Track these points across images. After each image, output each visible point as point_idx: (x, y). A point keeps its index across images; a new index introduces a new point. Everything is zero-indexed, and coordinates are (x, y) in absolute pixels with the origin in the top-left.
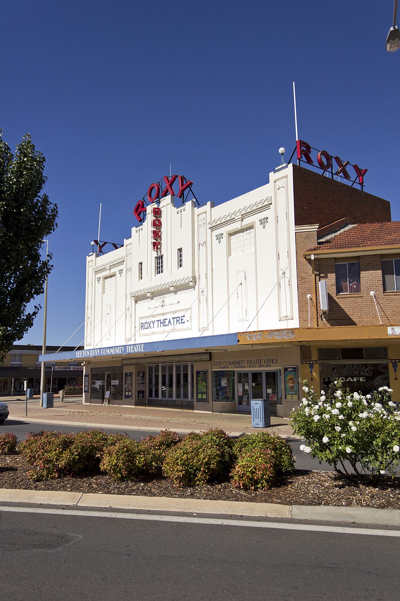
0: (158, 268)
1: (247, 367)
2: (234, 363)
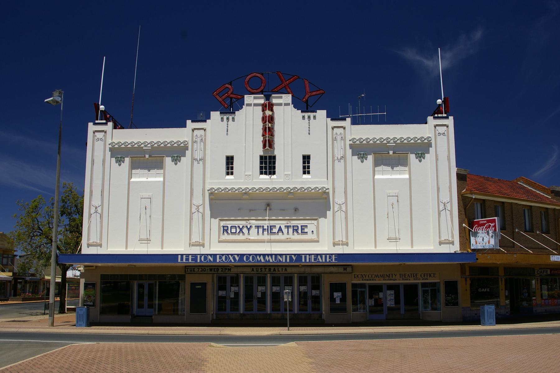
0: (304, 167)
1: (399, 280)
2: (383, 276)
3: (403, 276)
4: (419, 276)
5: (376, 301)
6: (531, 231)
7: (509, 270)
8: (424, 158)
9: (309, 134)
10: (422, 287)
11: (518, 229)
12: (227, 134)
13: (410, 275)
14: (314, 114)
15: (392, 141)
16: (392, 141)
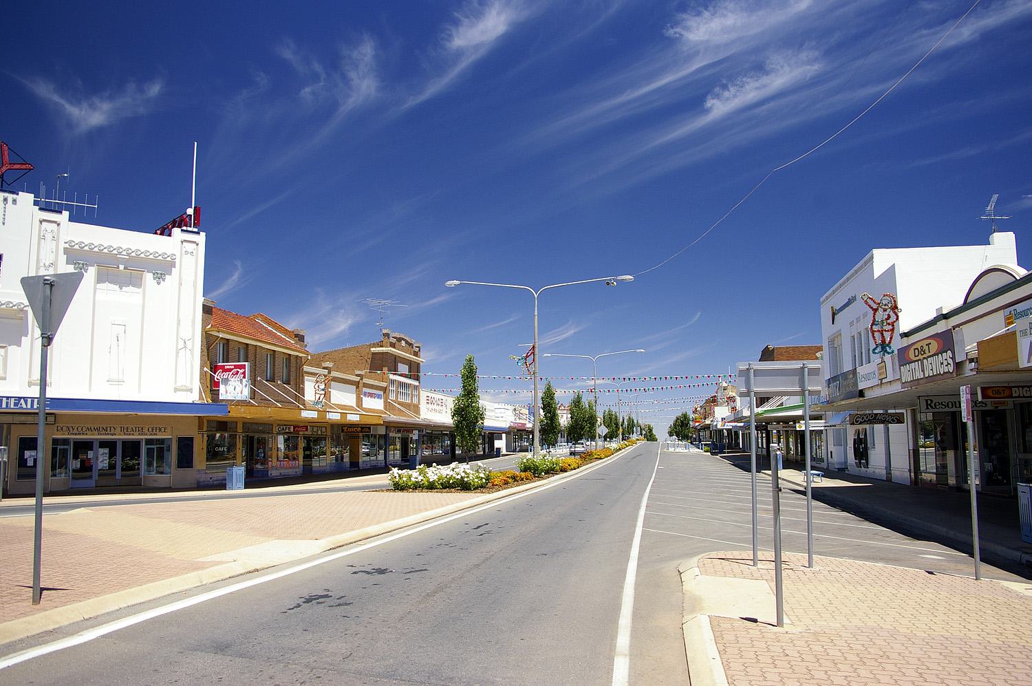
1: (120, 435)
2: (98, 429)
3: (124, 430)
4: (145, 430)
5: (83, 462)
6: (272, 380)
7: (249, 425)
8: (164, 280)
9: (4, 224)
10: (146, 444)
11: (261, 377)
12: (833, 323)
13: (134, 429)
14: (15, 196)
15: (124, 253)
16: (124, 253)
